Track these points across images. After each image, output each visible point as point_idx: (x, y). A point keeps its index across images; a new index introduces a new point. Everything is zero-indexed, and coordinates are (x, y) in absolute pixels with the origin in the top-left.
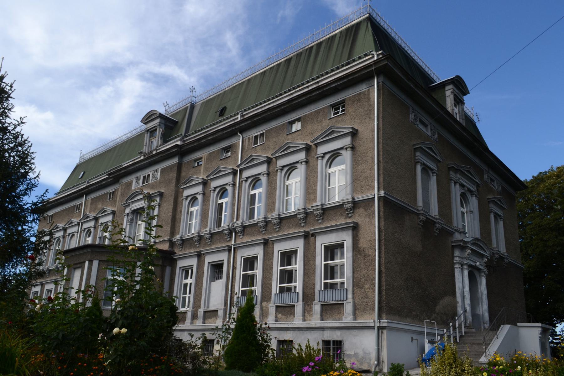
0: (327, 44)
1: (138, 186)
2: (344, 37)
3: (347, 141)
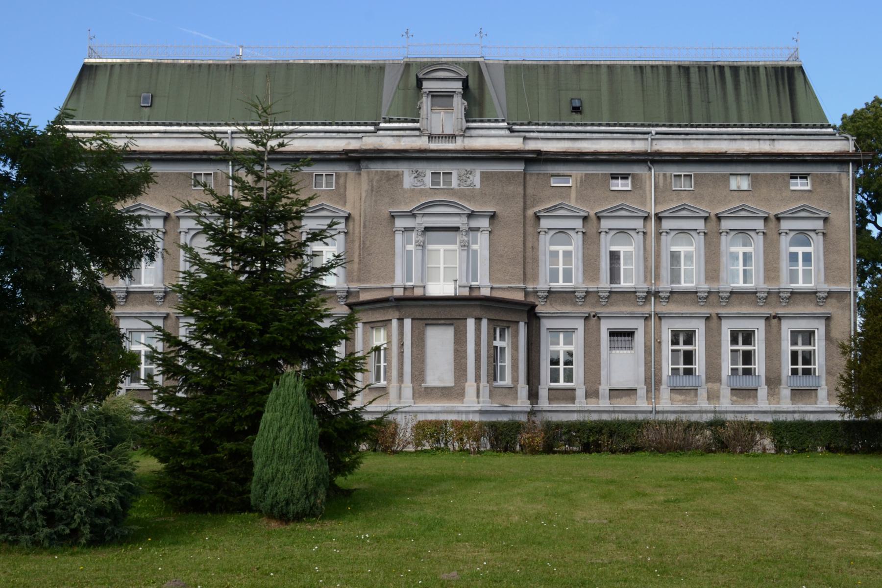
0: (749, 74)
1: (422, 187)
2: (773, 78)
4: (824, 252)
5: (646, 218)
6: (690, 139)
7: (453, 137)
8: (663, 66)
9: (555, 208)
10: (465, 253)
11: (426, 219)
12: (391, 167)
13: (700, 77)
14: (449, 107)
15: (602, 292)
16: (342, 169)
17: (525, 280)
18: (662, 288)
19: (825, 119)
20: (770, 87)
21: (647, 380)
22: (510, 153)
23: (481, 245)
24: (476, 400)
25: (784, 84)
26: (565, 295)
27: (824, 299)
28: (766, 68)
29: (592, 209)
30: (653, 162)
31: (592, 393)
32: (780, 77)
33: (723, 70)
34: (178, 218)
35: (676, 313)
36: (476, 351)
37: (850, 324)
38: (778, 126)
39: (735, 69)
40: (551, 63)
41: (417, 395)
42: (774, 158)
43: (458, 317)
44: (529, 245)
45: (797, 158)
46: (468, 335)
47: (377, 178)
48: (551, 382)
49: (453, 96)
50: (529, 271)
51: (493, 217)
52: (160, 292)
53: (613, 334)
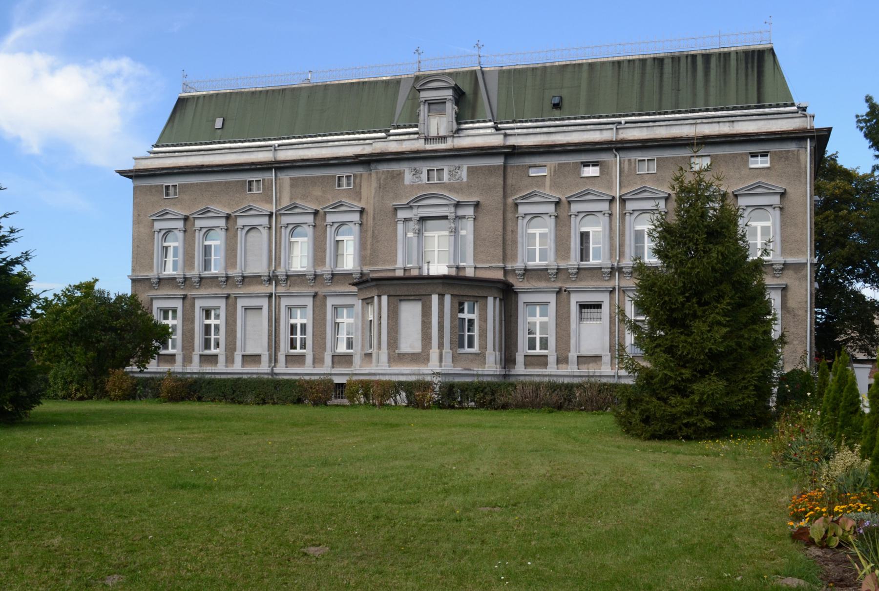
1: (420, 183)
3: (776, 200)
4: (781, 226)
5: (612, 201)
6: (681, 124)
7: (443, 138)
8: (640, 60)
9: (530, 195)
10: (452, 238)
11: (420, 210)
12: (395, 167)
13: (673, 67)
14: (442, 113)
15: (571, 269)
16: (358, 170)
17: (504, 259)
18: (623, 264)
19: (791, 98)
20: (739, 72)
21: (612, 348)
22: (488, 149)
23: (467, 230)
24: (438, 364)
25: (753, 67)
26: (539, 272)
27: (780, 270)
28: (737, 53)
29: (564, 195)
30: (618, 150)
31: (562, 360)
32: (750, 60)
33: (696, 59)
34: (325, 213)
35: (339, 292)
36: (439, 323)
37: (807, 295)
38: (742, 108)
39: (707, 57)
40: (539, 65)
41: (392, 360)
42: (729, 139)
43: (424, 293)
44: (509, 229)
45: (752, 138)
46: (433, 309)
47: (384, 176)
48: (529, 349)
49: (445, 102)
50: (509, 252)
51: (477, 205)
52: (223, 277)
53: (583, 306)
